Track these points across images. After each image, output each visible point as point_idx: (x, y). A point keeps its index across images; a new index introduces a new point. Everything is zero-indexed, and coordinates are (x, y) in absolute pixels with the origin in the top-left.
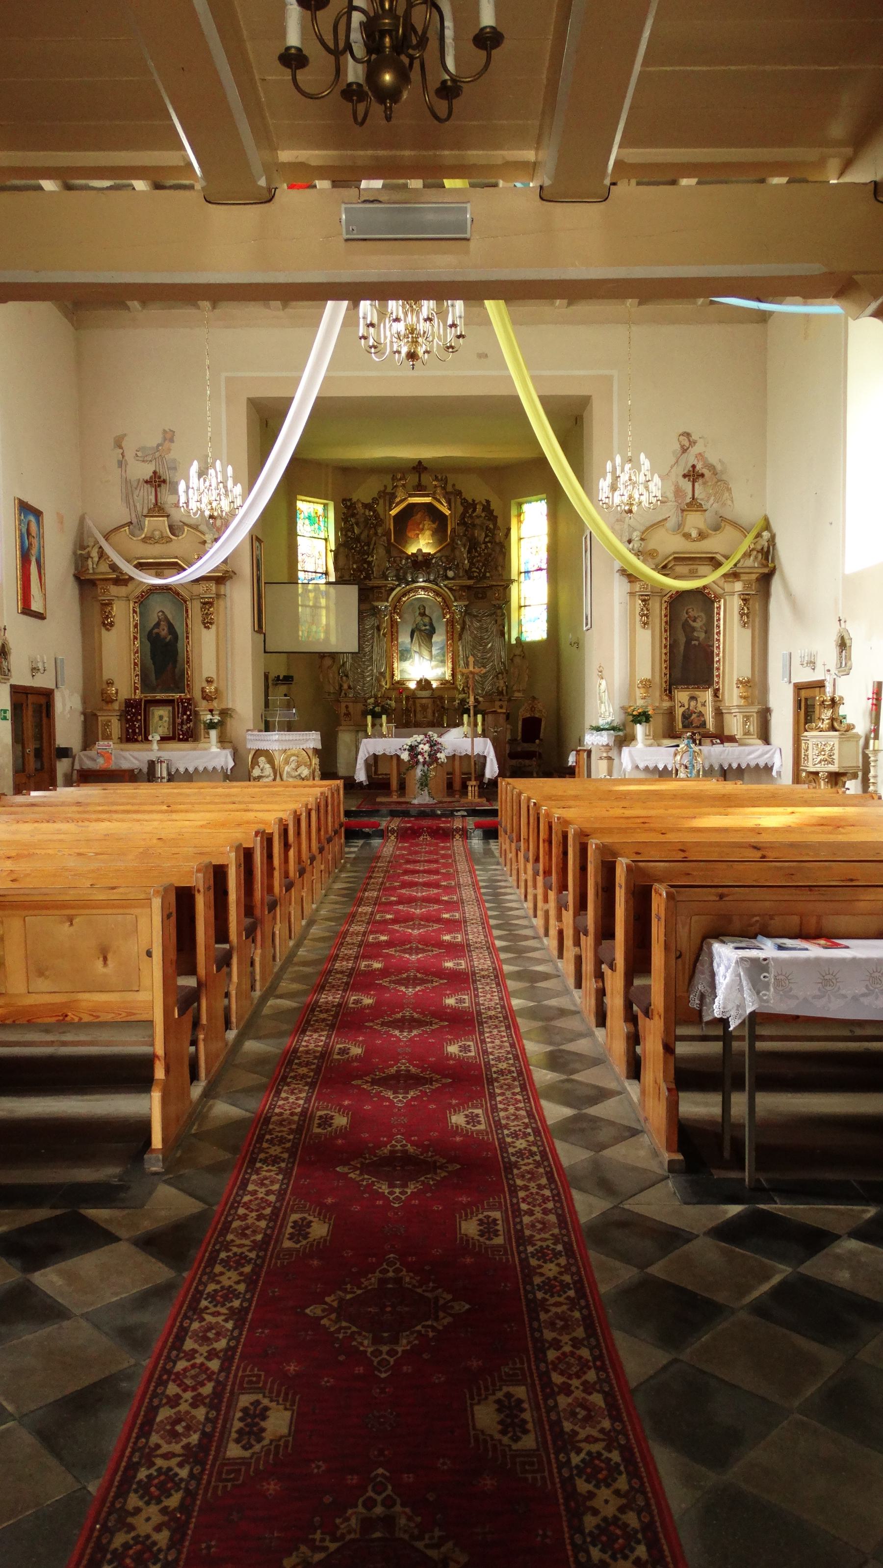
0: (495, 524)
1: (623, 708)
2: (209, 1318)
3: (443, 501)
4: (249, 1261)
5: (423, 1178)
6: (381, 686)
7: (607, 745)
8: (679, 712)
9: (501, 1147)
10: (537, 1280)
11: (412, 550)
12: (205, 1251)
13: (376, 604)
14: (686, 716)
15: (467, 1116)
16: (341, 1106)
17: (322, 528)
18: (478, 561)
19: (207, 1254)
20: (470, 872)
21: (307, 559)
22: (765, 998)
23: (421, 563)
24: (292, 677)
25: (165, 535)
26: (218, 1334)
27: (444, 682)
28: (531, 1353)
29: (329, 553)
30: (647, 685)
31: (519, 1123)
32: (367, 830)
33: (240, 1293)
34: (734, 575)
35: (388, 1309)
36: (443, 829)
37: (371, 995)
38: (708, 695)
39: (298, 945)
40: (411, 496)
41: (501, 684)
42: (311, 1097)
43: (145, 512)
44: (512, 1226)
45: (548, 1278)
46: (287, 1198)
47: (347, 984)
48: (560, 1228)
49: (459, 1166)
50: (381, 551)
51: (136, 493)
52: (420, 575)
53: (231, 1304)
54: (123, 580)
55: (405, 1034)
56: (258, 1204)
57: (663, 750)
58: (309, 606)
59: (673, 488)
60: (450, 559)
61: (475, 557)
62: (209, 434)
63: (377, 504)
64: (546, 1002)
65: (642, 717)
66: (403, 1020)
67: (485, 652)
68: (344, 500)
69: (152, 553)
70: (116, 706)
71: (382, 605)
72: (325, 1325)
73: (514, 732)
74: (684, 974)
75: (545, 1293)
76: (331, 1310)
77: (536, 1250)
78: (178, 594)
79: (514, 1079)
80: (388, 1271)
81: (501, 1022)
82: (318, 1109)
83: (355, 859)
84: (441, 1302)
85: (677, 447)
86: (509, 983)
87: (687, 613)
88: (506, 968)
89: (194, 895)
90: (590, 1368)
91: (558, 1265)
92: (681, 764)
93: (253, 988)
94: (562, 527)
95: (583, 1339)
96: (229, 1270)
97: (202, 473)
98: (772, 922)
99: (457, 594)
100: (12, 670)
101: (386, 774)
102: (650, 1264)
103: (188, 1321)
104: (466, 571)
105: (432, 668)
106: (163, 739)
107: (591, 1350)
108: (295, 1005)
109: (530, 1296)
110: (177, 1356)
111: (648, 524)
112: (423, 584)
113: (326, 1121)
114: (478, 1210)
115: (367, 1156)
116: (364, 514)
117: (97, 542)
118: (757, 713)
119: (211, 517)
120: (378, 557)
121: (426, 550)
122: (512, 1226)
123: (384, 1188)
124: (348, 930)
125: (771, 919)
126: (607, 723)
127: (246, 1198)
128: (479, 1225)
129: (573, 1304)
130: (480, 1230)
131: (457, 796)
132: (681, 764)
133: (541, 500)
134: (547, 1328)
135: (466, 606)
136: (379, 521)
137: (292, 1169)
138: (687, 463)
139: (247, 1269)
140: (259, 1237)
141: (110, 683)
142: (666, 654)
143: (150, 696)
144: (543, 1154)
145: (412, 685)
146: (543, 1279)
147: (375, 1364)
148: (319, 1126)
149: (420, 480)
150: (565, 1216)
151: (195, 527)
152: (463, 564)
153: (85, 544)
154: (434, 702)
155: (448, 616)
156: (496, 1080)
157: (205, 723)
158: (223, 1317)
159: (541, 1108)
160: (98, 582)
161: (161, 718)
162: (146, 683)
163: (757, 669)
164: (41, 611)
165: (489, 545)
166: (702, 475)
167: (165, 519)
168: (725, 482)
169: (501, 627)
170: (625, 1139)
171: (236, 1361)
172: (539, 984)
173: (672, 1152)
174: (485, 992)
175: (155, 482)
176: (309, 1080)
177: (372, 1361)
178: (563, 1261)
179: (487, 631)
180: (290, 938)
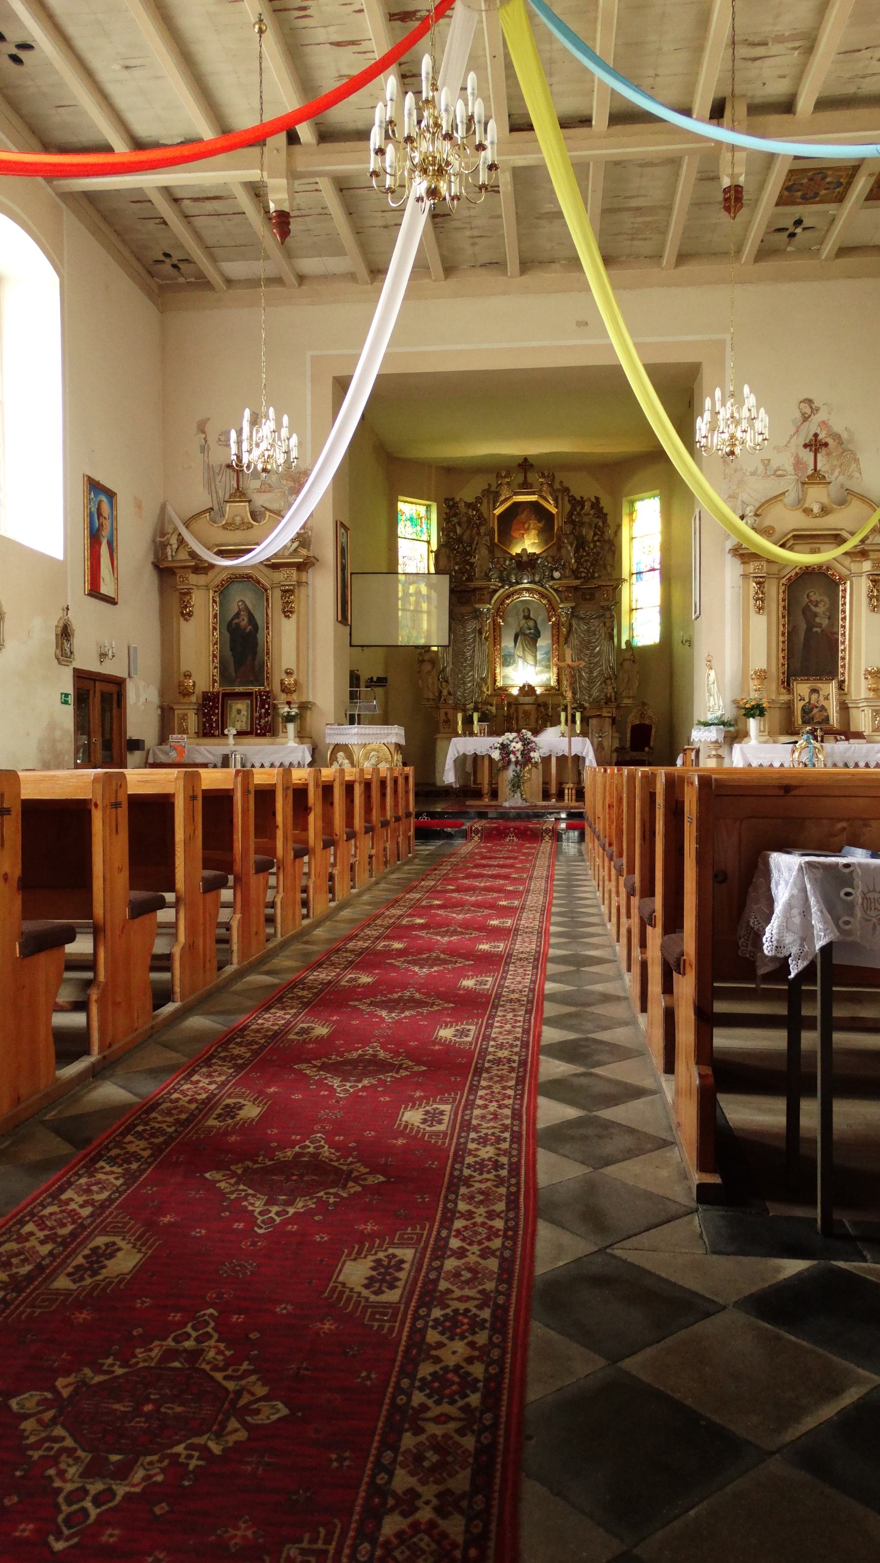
0: (605, 522)
1: (735, 702)
6: (483, 692)
7: (716, 742)
8: (799, 706)
11: (516, 550)
13: (477, 606)
14: (806, 711)
17: (425, 530)
18: (587, 561)
21: (408, 562)
22: (847, 927)
23: (527, 563)
27: (548, 688)
30: (762, 676)
31: (495, 1125)
34: (862, 553)
36: (531, 830)
37: (440, 1044)
40: (516, 494)
47: (351, 962)
49: (382, 1179)
50: (484, 551)
51: (218, 478)
52: (525, 577)
54: (202, 568)
58: (409, 610)
59: (792, 460)
60: (556, 560)
61: (582, 556)
62: (264, 380)
63: (481, 503)
65: (756, 711)
69: (232, 539)
70: (193, 699)
71: (484, 608)
73: (621, 740)
78: (259, 582)
79: (512, 1069)
81: (523, 1005)
83: (428, 855)
85: (798, 415)
87: (808, 596)
94: (676, 523)
97: (255, 421)
98: (866, 830)
99: (563, 595)
100: (75, 652)
106: (240, 734)
111: (763, 500)
112: (527, 586)
113: (231, 1111)
116: (467, 513)
117: (176, 529)
119: (264, 470)
120: (481, 557)
121: (530, 550)
124: (383, 913)
125: (865, 825)
126: (716, 718)
133: (654, 497)
135: (573, 608)
138: (808, 431)
141: (188, 675)
142: (783, 642)
143: (228, 689)
145: (515, 691)
149: (525, 477)
152: (570, 563)
155: (554, 619)
157: (283, 716)
160: (177, 571)
161: (239, 712)
162: (225, 676)
164: (112, 595)
167: (247, 504)
168: (853, 453)
169: (610, 630)
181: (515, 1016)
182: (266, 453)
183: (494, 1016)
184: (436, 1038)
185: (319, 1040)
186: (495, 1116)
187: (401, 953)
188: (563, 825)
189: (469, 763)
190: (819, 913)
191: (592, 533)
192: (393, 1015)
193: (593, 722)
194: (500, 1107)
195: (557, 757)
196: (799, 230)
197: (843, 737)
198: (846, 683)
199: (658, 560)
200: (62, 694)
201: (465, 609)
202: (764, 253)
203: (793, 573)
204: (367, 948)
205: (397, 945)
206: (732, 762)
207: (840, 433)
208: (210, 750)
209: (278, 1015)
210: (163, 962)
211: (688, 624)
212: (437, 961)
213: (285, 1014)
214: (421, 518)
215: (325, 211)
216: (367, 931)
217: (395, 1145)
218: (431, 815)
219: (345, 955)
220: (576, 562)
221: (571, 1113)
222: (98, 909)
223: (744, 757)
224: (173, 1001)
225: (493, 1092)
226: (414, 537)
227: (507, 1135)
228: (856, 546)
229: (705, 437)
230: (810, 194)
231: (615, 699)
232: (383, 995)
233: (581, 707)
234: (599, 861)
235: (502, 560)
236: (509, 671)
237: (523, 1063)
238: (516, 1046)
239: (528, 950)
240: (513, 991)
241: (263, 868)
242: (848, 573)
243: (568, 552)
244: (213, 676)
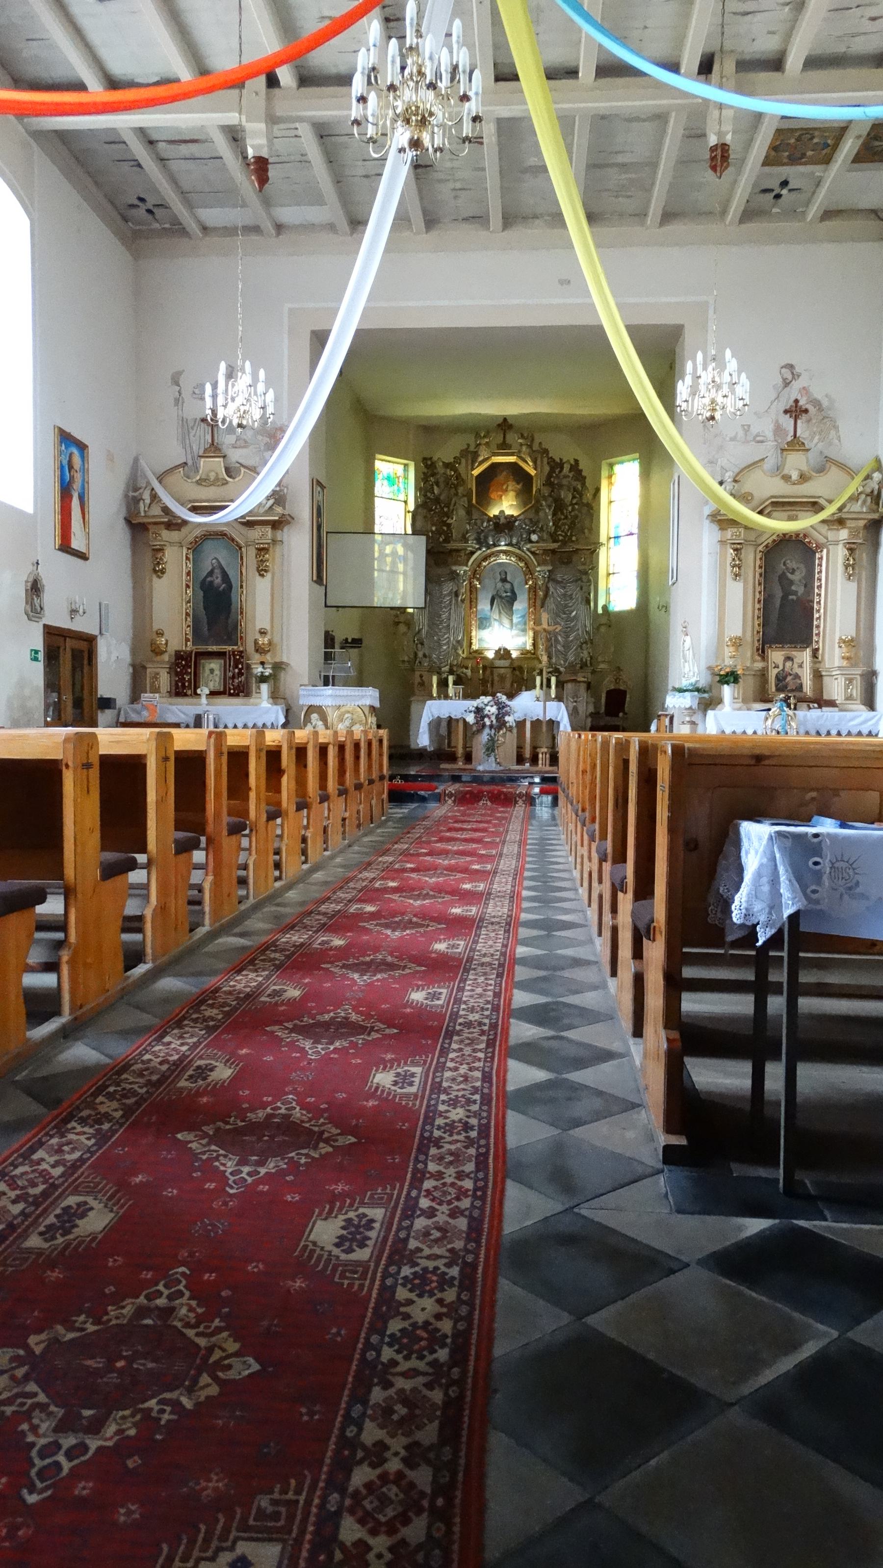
0: (583, 484)
1: (709, 668)
6: (458, 655)
7: (690, 708)
8: (773, 673)
11: (494, 512)
13: (454, 568)
14: (780, 678)
16: (233, 1054)
17: (402, 489)
18: (564, 524)
20: (521, 832)
23: (504, 525)
27: (524, 652)
30: (737, 643)
32: (422, 793)
35: (120, 1364)
36: (505, 794)
37: (411, 1006)
41: (585, 655)
47: (325, 924)
48: (468, 1239)
49: (353, 1140)
50: (462, 512)
51: (192, 433)
54: (175, 524)
56: (445, 1193)
57: (753, 713)
59: (772, 427)
61: (560, 519)
62: (240, 333)
63: (460, 464)
64: (559, 952)
65: (731, 677)
67: (569, 619)
68: (425, 459)
69: (205, 495)
70: (166, 657)
71: (461, 570)
73: (596, 705)
78: (233, 540)
79: (483, 1033)
83: (401, 818)
87: (785, 564)
89: (61, 772)
91: (440, 1301)
94: (655, 489)
97: (230, 375)
98: (836, 799)
100: (45, 608)
106: (213, 694)
107: (437, 1470)
111: (743, 466)
112: (504, 548)
113: (203, 1072)
117: (148, 483)
118: (861, 675)
119: (240, 425)
120: (458, 518)
121: (508, 512)
124: (355, 876)
126: (691, 684)
131: (528, 765)
133: (634, 460)
135: (549, 571)
141: (160, 634)
142: (759, 609)
143: (202, 648)
145: (490, 655)
146: (406, 1324)
152: (547, 525)
153: (139, 486)
155: (530, 583)
156: (458, 1033)
157: (256, 676)
160: (150, 527)
161: (212, 671)
163: (862, 625)
164: (83, 550)
166: (806, 411)
167: (221, 459)
168: (833, 421)
169: (587, 594)
172: (554, 933)
174: (489, 938)
181: (486, 979)
182: (242, 409)
183: (466, 980)
184: (408, 1001)
185: (291, 1002)
186: (466, 1079)
187: (373, 916)
188: (537, 790)
189: (444, 724)
190: (787, 882)
191: (570, 496)
192: (365, 978)
193: (569, 686)
194: (470, 1069)
195: (532, 722)
196: (784, 192)
197: (816, 705)
198: (820, 651)
200: (32, 650)
201: (440, 571)
202: (749, 214)
203: (770, 540)
204: (339, 911)
205: (370, 908)
206: (706, 729)
208: (182, 710)
209: (250, 977)
210: (134, 924)
211: (665, 590)
212: (410, 924)
213: (257, 976)
214: (398, 478)
215: (304, 158)
216: (340, 894)
218: (405, 778)
219: (317, 917)
220: (554, 524)
221: (540, 1075)
222: (69, 871)
224: (145, 963)
225: (463, 1055)
226: (391, 496)
227: (477, 1097)
228: (833, 514)
229: (686, 401)
231: (591, 664)
232: (354, 958)
233: (556, 672)
234: (571, 826)
235: (479, 522)
237: (493, 1026)
238: (487, 1009)
239: (500, 914)
240: (485, 955)
241: (236, 830)
244: (186, 634)
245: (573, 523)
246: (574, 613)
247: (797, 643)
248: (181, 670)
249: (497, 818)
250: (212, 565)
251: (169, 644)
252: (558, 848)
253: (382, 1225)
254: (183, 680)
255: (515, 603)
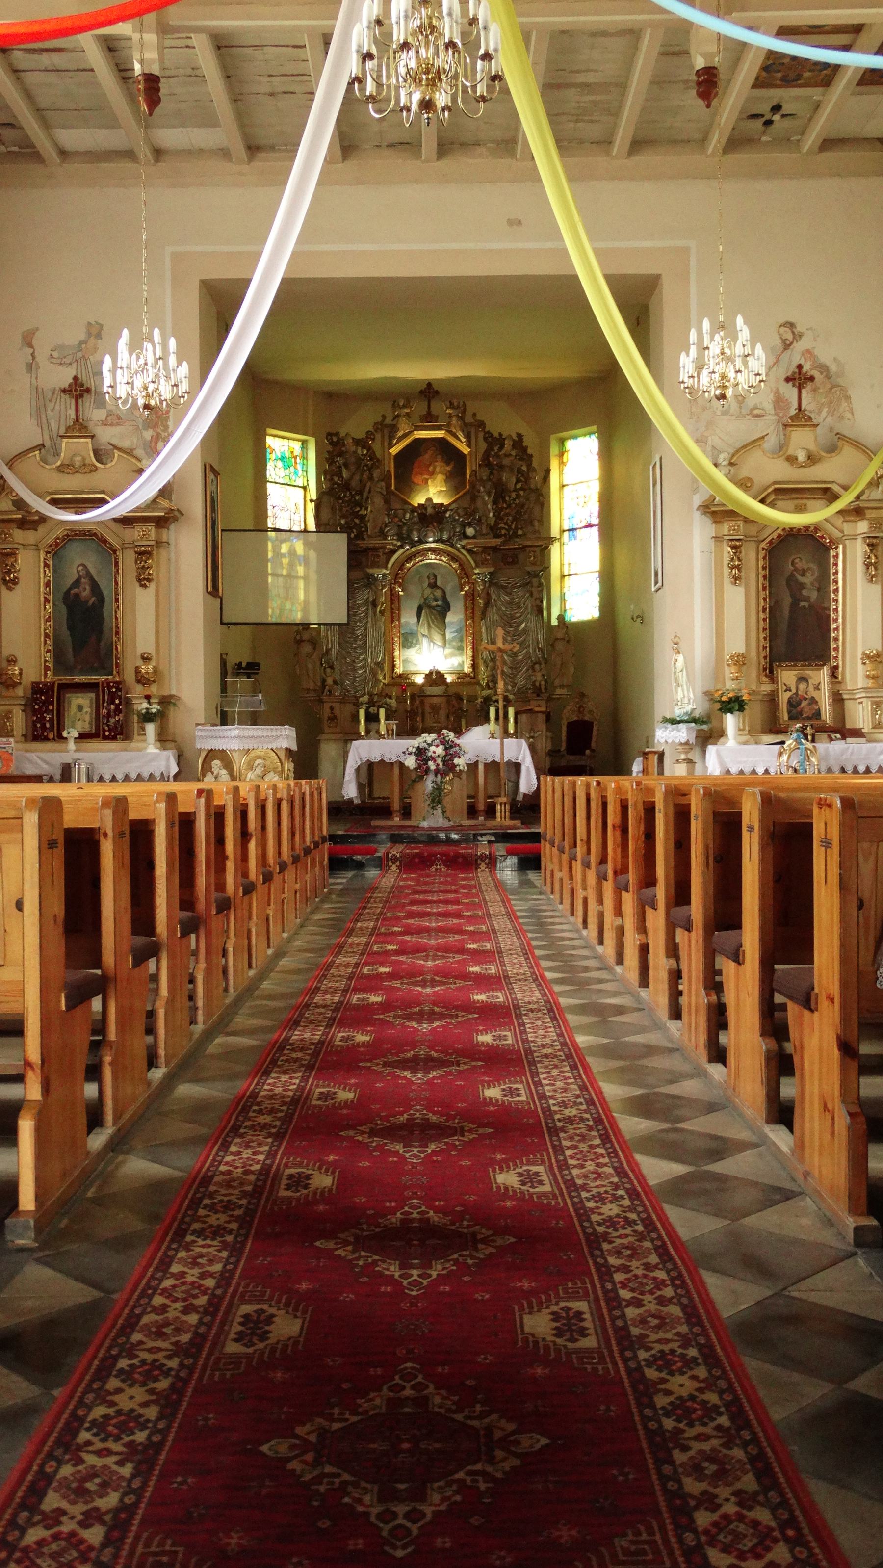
0: (529, 466)
1: (707, 693)
2: (91, 1460)
3: (461, 435)
4: (167, 1373)
5: (455, 1256)
6: (377, 681)
7: (687, 743)
8: (784, 698)
9: (579, 1215)
10: (661, 1401)
11: (419, 499)
12: (95, 1357)
13: (370, 571)
14: (793, 704)
15: (520, 1175)
16: (323, 1163)
17: (300, 472)
18: (508, 515)
19: (96, 1362)
20: (503, 901)
21: (279, 513)
24: (258, 665)
25: (87, 462)
26: (104, 1485)
28: (666, 1515)
29: (309, 503)
30: (740, 661)
33: (148, 1421)
34: (856, 512)
36: (463, 856)
38: (824, 675)
39: (262, 976)
41: (538, 677)
42: (276, 1151)
43: (62, 431)
44: (608, 1323)
45: (680, 1398)
46: (234, 1282)
48: (688, 1322)
50: (379, 501)
51: (50, 406)
53: (131, 1438)
55: (420, 1076)
57: (762, 748)
59: (771, 396)
60: (470, 513)
61: (502, 509)
62: (145, 294)
63: (373, 440)
64: (627, 1039)
65: (734, 704)
66: (416, 1059)
68: (329, 435)
70: (20, 692)
71: (379, 573)
72: (294, 1471)
73: (555, 740)
74: (867, 939)
75: (679, 1421)
76: (305, 1446)
77: (653, 1356)
78: (105, 541)
80: (404, 1388)
82: (286, 1166)
83: (342, 890)
84: (498, 1434)
85: (778, 342)
86: (569, 1017)
87: (793, 564)
88: (563, 1001)
90: (776, 1541)
92: (788, 767)
93: (193, 1021)
94: (619, 469)
95: (756, 1494)
96: (131, 1386)
97: (135, 346)
101: (384, 798)
102: (854, 1376)
103: (53, 1463)
104: (491, 528)
105: (446, 657)
108: (254, 1043)
109: (653, 1425)
110: (29, 1519)
111: (738, 445)
112: (433, 545)
113: (299, 1181)
114: (549, 1300)
115: (365, 1226)
119: (147, 406)
121: (436, 501)
122: (608, 1323)
123: (394, 1270)
124: (333, 962)
126: (686, 714)
127: (167, 1283)
128: (553, 1320)
129: (729, 1438)
130: (556, 1328)
131: (481, 818)
132: (788, 767)
133: (590, 434)
134: (689, 1475)
135: (491, 574)
136: (375, 461)
137: (243, 1244)
139: (163, 1384)
140: (185, 1338)
141: (12, 661)
142: (764, 620)
143: (66, 678)
144: (648, 1223)
145: (419, 680)
147: (385, 1533)
148: (288, 1187)
150: (694, 1307)
151: (129, 452)
152: (487, 517)
154: (448, 701)
155: (467, 588)
157: (139, 714)
158: (114, 1458)
159: (637, 1164)
161: (80, 708)
162: (60, 663)
165: (522, 493)
166: (812, 379)
167: (89, 440)
168: (843, 389)
169: (538, 602)
170: (772, 1203)
171: (134, 1528)
173: (862, 1215)
174: (536, 1029)
175: (76, 391)
176: (273, 1131)
177: (380, 1529)
178: (702, 1372)
179: (519, 607)
180: (250, 967)
181: (561, 1072)
191: (514, 480)
195: (486, 765)
196: (776, 118)
197: (838, 736)
199: (596, 513)
203: (775, 535)
206: (706, 768)
207: (828, 364)
214: (295, 457)
215: (197, 72)
217: (505, 1207)
221: (679, 1169)
223: (721, 762)
224: (157, 1067)
229: (692, 377)
230: (792, 75)
231: (546, 689)
235: (400, 512)
236: (411, 654)
237: (598, 1121)
242: (840, 535)
243: (486, 504)
244: (46, 661)
245: (519, 513)
246: (523, 626)
247: (797, 660)
248: (40, 707)
249: (464, 887)
250: (78, 572)
251: (24, 675)
252: (557, 920)
253: (592, 1314)
254: (42, 720)
255: (449, 614)
